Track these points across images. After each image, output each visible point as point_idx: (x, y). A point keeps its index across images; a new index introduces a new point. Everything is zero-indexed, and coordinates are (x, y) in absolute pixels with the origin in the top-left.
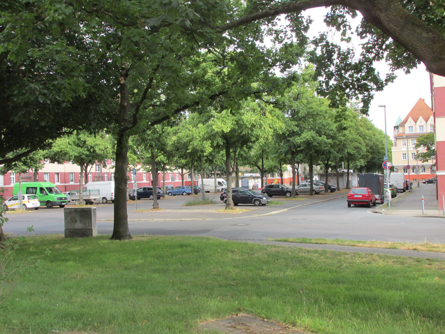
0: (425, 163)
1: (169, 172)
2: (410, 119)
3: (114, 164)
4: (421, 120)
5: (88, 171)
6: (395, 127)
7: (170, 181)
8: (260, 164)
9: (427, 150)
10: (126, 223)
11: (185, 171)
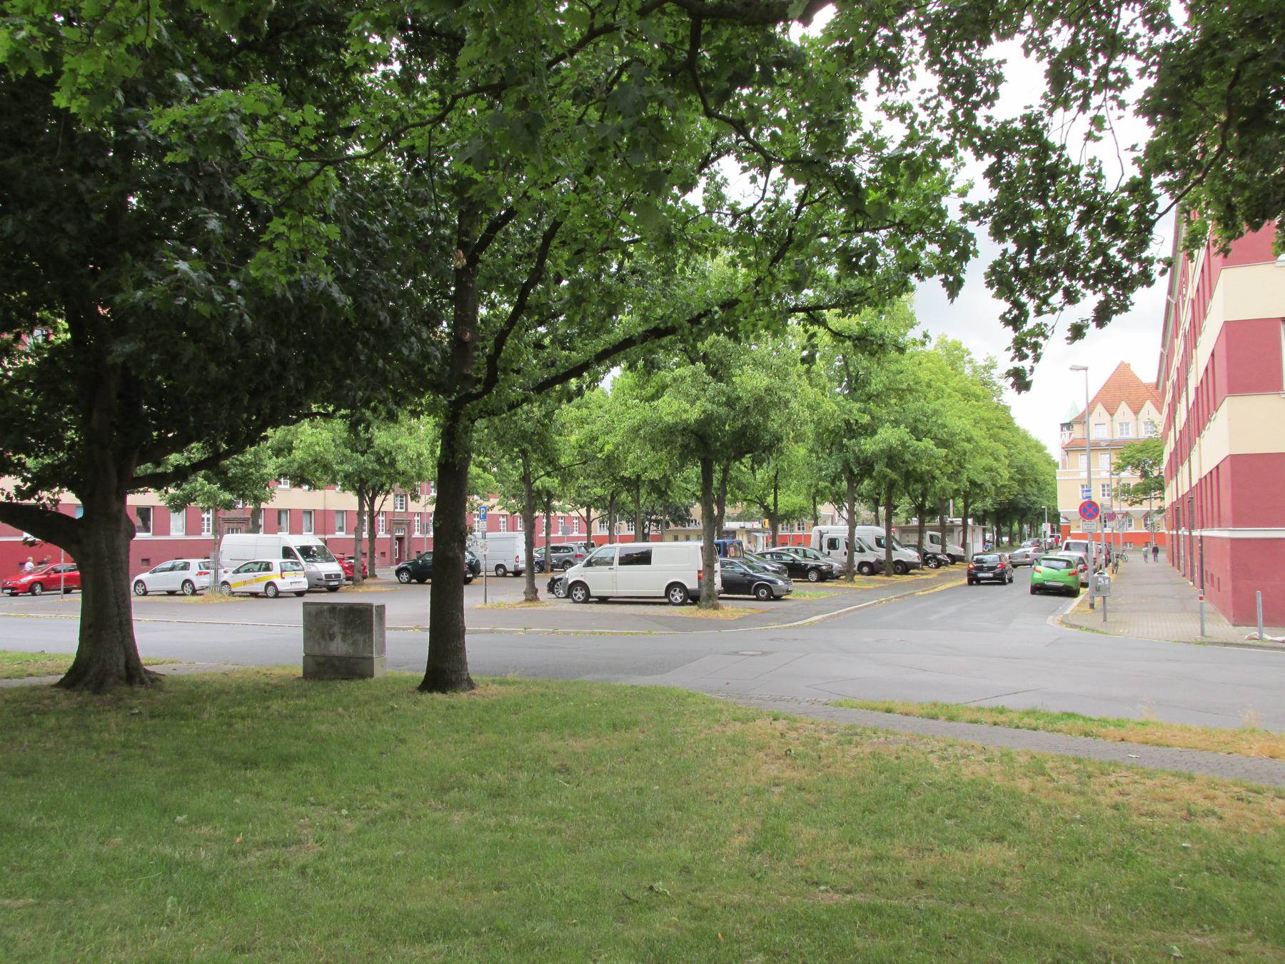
0: (1137, 508)
1: (559, 514)
2: (1099, 408)
3: (434, 494)
4: (1124, 410)
5: (376, 509)
6: (1063, 425)
7: (560, 534)
8: (770, 500)
9: (1141, 477)
10: (461, 649)
11: (594, 514)
